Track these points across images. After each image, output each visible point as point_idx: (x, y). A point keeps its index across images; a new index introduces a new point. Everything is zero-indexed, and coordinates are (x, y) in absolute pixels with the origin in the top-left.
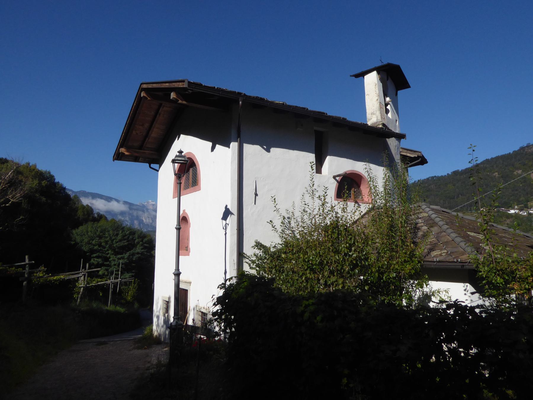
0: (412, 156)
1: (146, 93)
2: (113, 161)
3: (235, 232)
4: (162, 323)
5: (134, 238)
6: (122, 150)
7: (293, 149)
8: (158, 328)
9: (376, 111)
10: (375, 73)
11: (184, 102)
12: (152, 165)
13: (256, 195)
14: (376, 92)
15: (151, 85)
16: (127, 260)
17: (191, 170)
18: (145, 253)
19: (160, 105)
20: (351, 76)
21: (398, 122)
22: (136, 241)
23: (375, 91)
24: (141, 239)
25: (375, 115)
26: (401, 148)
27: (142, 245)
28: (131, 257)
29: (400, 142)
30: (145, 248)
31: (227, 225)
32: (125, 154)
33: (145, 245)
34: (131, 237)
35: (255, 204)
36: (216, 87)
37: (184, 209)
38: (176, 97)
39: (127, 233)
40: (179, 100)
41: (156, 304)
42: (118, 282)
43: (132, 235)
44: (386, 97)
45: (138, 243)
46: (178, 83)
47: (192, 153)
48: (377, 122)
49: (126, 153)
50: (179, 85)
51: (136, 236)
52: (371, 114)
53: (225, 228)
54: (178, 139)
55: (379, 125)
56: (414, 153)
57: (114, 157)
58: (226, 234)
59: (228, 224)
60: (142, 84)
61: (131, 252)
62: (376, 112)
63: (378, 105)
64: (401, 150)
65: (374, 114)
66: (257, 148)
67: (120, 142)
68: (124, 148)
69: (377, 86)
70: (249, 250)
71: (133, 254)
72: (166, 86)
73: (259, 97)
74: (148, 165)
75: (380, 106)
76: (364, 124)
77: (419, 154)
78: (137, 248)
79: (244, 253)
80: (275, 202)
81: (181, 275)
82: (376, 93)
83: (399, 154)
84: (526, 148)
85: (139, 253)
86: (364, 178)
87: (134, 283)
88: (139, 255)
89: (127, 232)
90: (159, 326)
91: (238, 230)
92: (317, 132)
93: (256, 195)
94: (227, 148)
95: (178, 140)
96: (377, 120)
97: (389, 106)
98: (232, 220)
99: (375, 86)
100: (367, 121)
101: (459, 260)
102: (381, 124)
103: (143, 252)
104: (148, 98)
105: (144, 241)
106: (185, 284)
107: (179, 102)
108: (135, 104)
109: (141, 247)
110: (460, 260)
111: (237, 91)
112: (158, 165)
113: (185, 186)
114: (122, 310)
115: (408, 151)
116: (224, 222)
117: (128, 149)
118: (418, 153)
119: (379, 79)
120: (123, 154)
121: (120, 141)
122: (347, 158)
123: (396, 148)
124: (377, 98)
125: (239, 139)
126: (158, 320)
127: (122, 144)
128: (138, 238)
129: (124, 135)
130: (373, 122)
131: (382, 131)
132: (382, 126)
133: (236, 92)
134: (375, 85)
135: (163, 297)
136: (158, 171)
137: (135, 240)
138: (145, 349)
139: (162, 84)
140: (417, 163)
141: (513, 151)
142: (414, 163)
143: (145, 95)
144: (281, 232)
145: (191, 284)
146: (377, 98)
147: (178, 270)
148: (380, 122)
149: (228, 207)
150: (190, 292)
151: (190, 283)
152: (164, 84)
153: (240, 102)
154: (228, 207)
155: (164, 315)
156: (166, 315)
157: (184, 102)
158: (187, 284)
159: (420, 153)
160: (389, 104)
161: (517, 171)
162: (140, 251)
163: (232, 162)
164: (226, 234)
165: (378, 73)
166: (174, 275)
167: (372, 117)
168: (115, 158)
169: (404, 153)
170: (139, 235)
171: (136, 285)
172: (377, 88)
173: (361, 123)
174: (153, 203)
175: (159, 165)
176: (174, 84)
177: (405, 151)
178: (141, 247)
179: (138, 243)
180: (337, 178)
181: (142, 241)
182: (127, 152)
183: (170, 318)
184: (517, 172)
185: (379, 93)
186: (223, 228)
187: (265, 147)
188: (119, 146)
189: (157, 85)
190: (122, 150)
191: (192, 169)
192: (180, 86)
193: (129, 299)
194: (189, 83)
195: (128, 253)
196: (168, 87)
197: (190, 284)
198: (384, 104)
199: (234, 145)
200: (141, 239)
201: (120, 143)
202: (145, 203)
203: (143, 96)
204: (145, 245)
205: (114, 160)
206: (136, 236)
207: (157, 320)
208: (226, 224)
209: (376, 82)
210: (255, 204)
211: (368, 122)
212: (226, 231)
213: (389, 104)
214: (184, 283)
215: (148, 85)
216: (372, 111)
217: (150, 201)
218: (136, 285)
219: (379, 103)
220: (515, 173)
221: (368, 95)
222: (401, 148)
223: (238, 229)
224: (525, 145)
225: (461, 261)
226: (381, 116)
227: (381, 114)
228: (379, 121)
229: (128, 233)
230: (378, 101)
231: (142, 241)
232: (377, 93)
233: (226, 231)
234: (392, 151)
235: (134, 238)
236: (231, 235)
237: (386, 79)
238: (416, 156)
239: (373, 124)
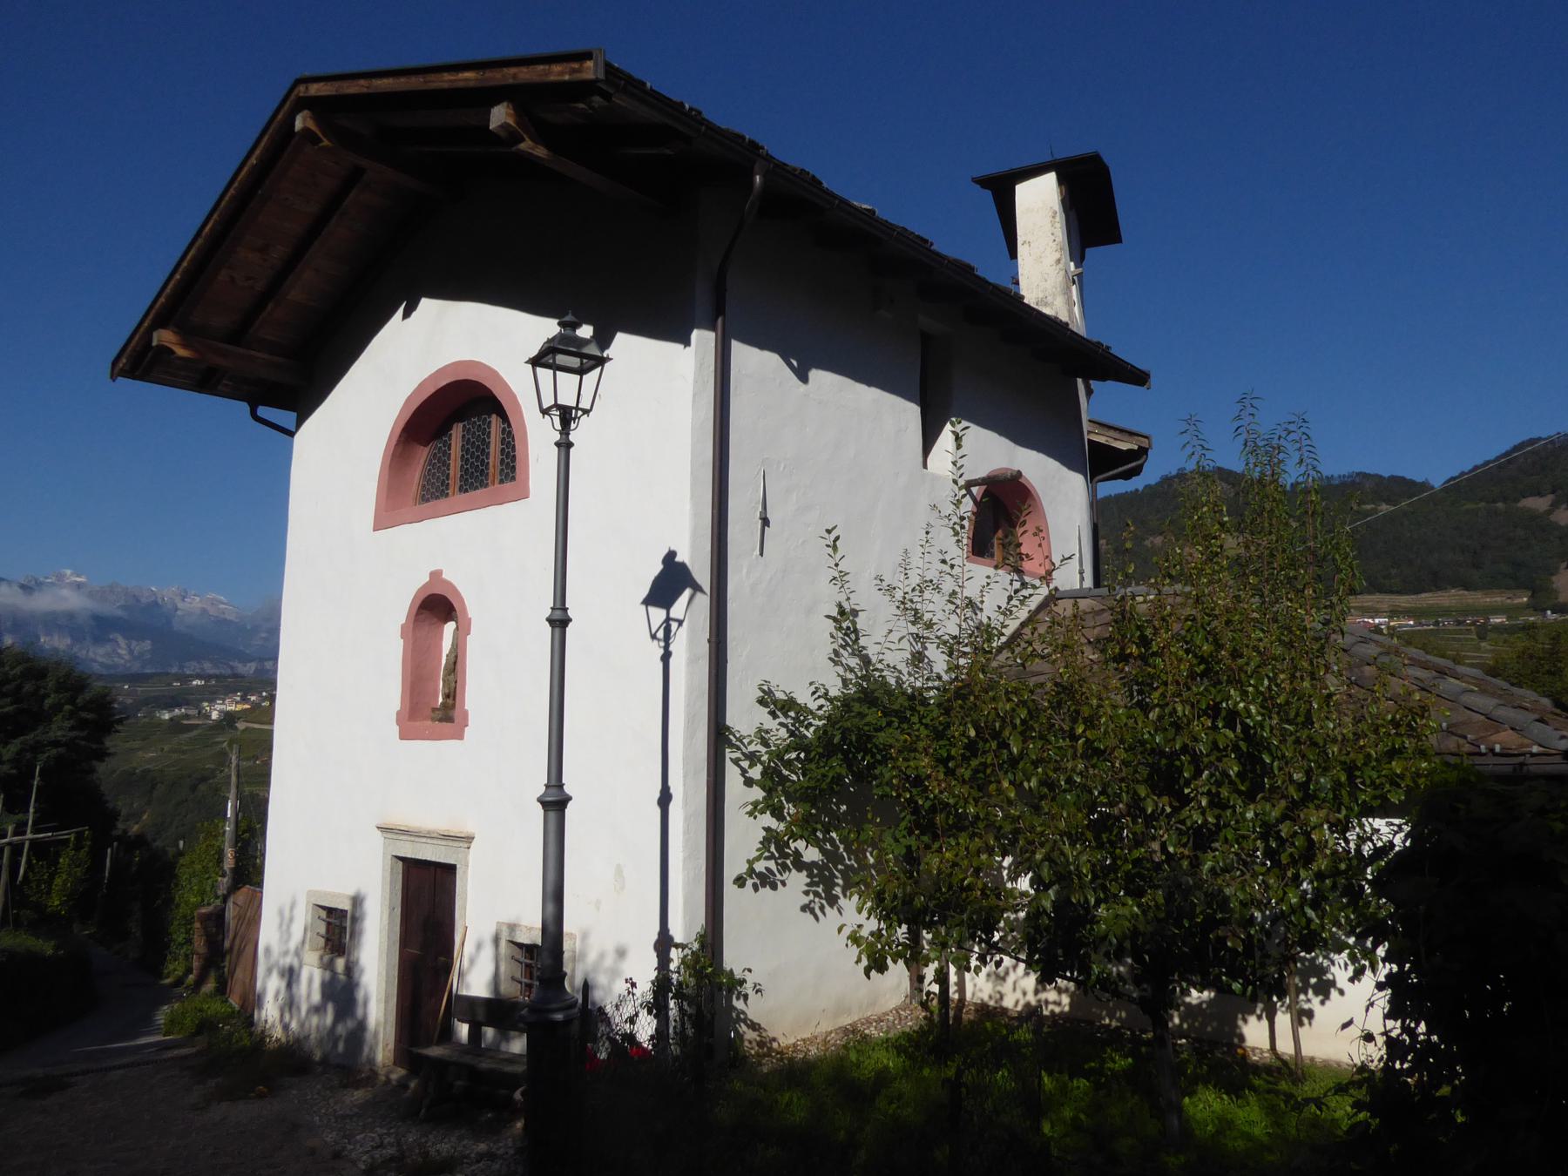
0: (1124, 446)
1: (317, 118)
2: (112, 377)
3: (704, 649)
4: (316, 997)
5: (42, 691)
6: (164, 337)
7: (870, 383)
8: (291, 1017)
10: (1050, 179)
11: (541, 152)
12: (263, 411)
13: (765, 522)
15: (362, 82)
16: (12, 768)
17: (457, 432)
18: (83, 743)
19: (355, 176)
22: (48, 702)
24: (68, 695)
27: (72, 714)
28: (29, 755)
30: (84, 723)
31: (674, 625)
32: (173, 352)
33: (84, 715)
34: (28, 687)
35: (761, 554)
36: (687, 106)
37: (433, 569)
38: (517, 124)
39: (12, 673)
40: (525, 136)
41: (281, 925)
42: (23, 844)
43: (33, 682)
45: (57, 708)
46: (541, 67)
47: (482, 364)
49: (181, 352)
50: (548, 74)
51: (51, 683)
53: (660, 634)
54: (407, 315)
56: (1130, 439)
57: (114, 363)
58: (666, 657)
59: (680, 623)
60: (299, 82)
61: (30, 737)
62: (1055, 299)
66: (772, 360)
67: (157, 306)
68: (174, 332)
69: (1058, 219)
70: (745, 717)
71: (37, 748)
72: (455, 80)
73: (808, 173)
74: (244, 407)
78: (54, 726)
79: (728, 728)
80: (835, 548)
81: (570, 805)
84: (1176, 480)
85: (59, 741)
86: (1034, 499)
87: (78, 848)
88: (60, 749)
89: (12, 669)
90: (299, 1009)
91: (714, 645)
92: (926, 339)
93: (765, 522)
94: (679, 347)
95: (406, 321)
98: (691, 610)
101: (1498, 748)
103: (76, 738)
104: (324, 140)
105: (78, 701)
106: (444, 843)
107: (522, 146)
108: (253, 160)
109: (67, 724)
110: (1502, 749)
111: (747, 137)
112: (294, 415)
113: (424, 486)
114: (47, 948)
116: (658, 615)
117: (187, 334)
120: (164, 351)
121: (151, 307)
122: (1000, 434)
124: (1057, 255)
125: (720, 320)
126: (289, 985)
127: (168, 311)
128: (57, 691)
129: (179, 281)
133: (743, 138)
135: (310, 893)
136: (291, 434)
137: (47, 696)
138: (261, 1096)
139: (432, 77)
140: (1125, 472)
141: (1146, 486)
142: (1121, 469)
143: (311, 125)
144: (833, 656)
145: (473, 845)
147: (560, 786)
149: (678, 559)
150: (465, 872)
151: (469, 839)
152: (447, 76)
153: (758, 177)
154: (678, 559)
155: (328, 966)
156: (340, 964)
157: (541, 152)
158: (451, 843)
159: (1146, 440)
161: (1151, 538)
162: (64, 736)
163: (694, 395)
164: (666, 657)
165: (1061, 181)
166: (540, 806)
168: (121, 369)
170: (62, 680)
171: (83, 853)
172: (1058, 225)
174: (78, 579)
175: (295, 414)
176: (513, 70)
178: (67, 724)
179: (57, 708)
180: (975, 490)
181: (72, 701)
182: (184, 346)
183: (360, 977)
184: (1152, 542)
186: (654, 637)
187: (795, 363)
188: (151, 316)
189: (403, 80)
190: (164, 337)
191: (461, 425)
192: (552, 78)
193: (57, 903)
194: (609, 67)
195: (17, 741)
196: (472, 84)
197: (466, 845)
199: (703, 339)
200: (68, 695)
201: (154, 311)
202: (47, 578)
203: (306, 130)
204: (84, 715)
205: (113, 378)
206: (51, 683)
207: (283, 984)
208: (668, 619)
210: (761, 554)
212: (666, 647)
214: (439, 842)
215: (337, 84)
216: (1041, 295)
217: (68, 572)
218: (83, 853)
220: (1147, 543)
221: (1026, 246)
223: (713, 639)
224: (1174, 473)
225: (1505, 751)
229: (18, 670)
231: (72, 701)
233: (666, 647)
235: (42, 691)
236: (692, 661)
238: (1136, 447)
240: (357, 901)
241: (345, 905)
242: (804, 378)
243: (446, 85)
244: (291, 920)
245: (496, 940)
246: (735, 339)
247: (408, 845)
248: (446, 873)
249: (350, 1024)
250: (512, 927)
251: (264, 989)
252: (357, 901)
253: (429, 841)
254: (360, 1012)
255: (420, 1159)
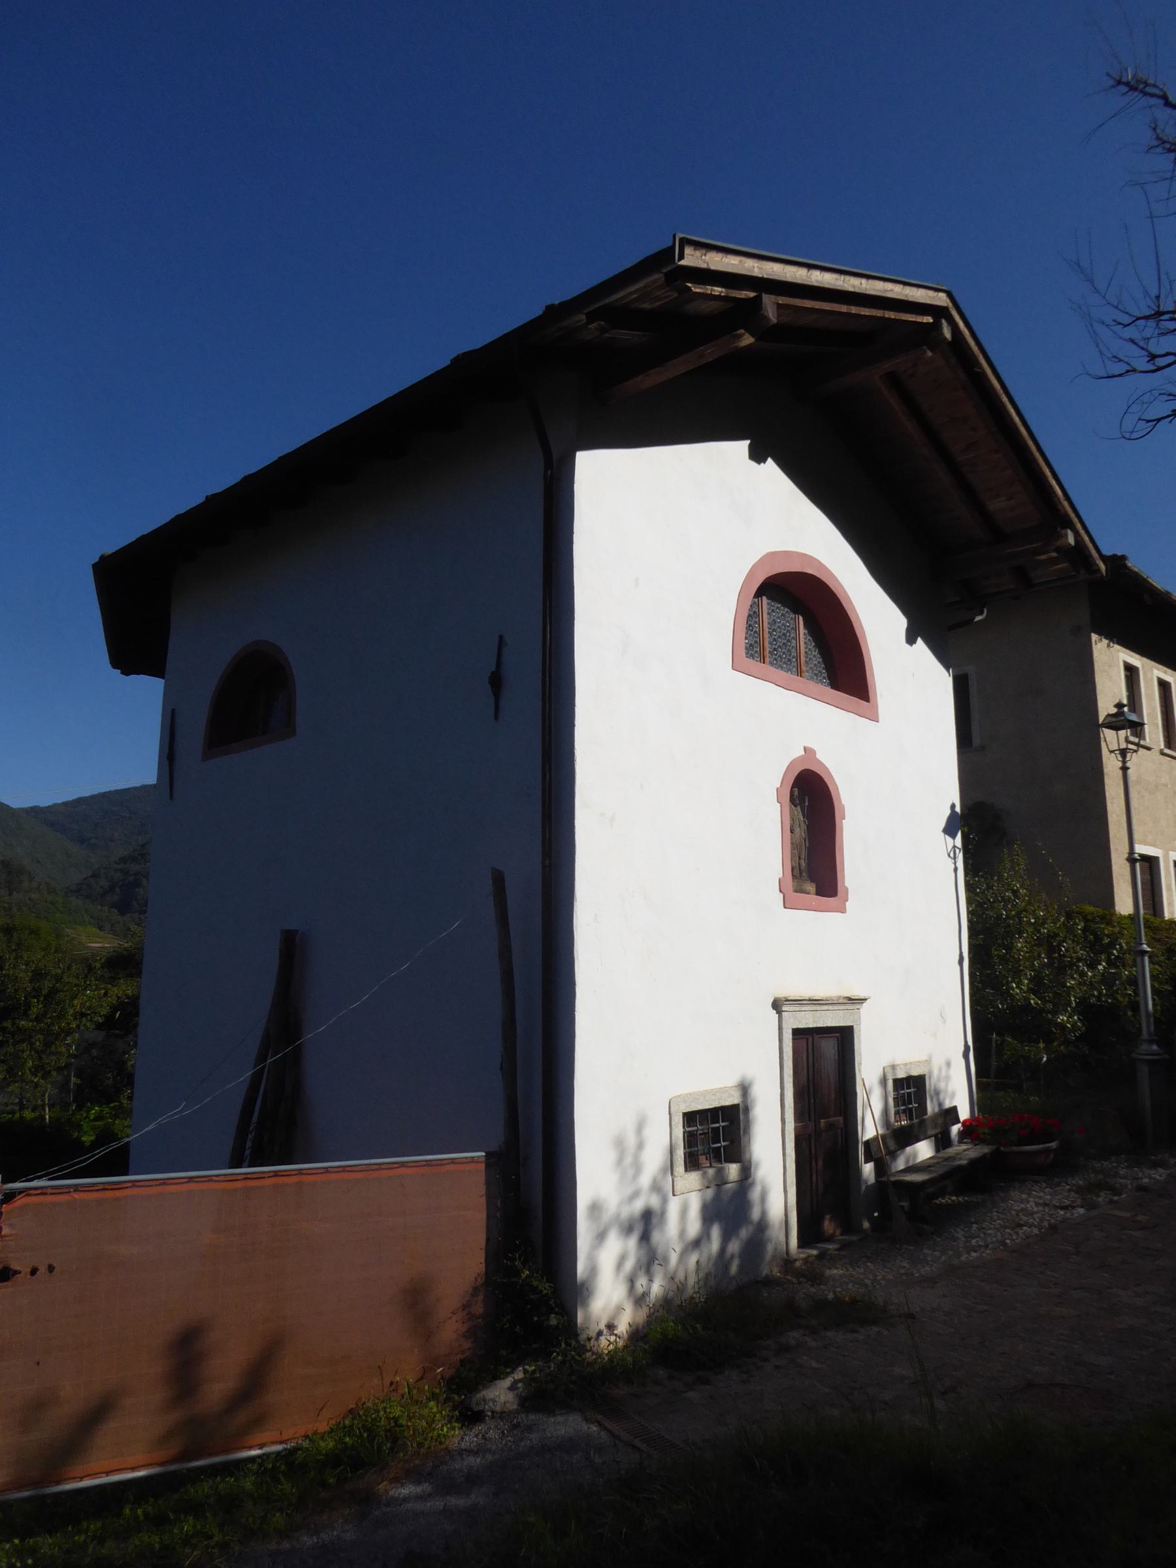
41: (620, 1161)
53: (952, 855)
186: (949, 855)
240: (744, 1089)
241: (733, 1099)
242: (911, 640)
243: (743, 297)
244: (640, 1146)
245: (883, 1081)
246: (922, 638)
247: (809, 1015)
248: (844, 1037)
249: (744, 1233)
250: (893, 1067)
251: (593, 1270)
252: (744, 1089)
253: (830, 1007)
254: (755, 1214)
255: (1080, 956)
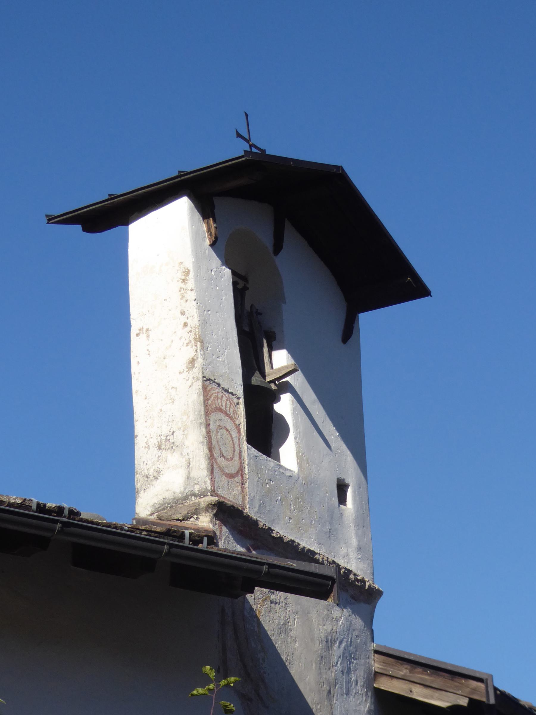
9: (185, 428)
14: (183, 319)
20: (51, 219)
21: (354, 492)
23: (183, 313)
25: (176, 455)
26: (376, 652)
29: (369, 621)
44: (271, 349)
48: (186, 498)
52: (159, 448)
55: (197, 512)
62: (186, 436)
63: (195, 396)
64: (377, 666)
65: (173, 447)
69: (191, 283)
75: (206, 400)
76: (41, 508)
77: (474, 690)
82: (185, 325)
83: (359, 688)
96: (186, 485)
97: (286, 399)
99: (184, 281)
100: (138, 485)
102: (210, 506)
115: (419, 669)
118: (474, 684)
119: (208, 242)
123: (337, 651)
130: (169, 496)
131: (168, 554)
132: (216, 516)
134: (180, 276)
146: (192, 354)
148: (203, 494)
159: (481, 685)
160: (287, 388)
167: (161, 466)
169: (395, 682)
172: (192, 296)
173: (19, 506)
177: (404, 671)
185: (204, 322)
198: (240, 391)
209: (189, 262)
211: (141, 494)
213: (287, 388)
216: (165, 430)
219: (199, 385)
221: (143, 336)
222: (376, 652)
226: (211, 457)
227: (210, 447)
228: (197, 489)
230: (197, 372)
232: (189, 322)
234: (294, 671)
237: (268, 241)
238: (464, 702)
239: (160, 509)
